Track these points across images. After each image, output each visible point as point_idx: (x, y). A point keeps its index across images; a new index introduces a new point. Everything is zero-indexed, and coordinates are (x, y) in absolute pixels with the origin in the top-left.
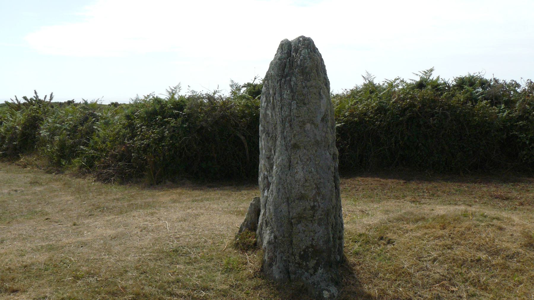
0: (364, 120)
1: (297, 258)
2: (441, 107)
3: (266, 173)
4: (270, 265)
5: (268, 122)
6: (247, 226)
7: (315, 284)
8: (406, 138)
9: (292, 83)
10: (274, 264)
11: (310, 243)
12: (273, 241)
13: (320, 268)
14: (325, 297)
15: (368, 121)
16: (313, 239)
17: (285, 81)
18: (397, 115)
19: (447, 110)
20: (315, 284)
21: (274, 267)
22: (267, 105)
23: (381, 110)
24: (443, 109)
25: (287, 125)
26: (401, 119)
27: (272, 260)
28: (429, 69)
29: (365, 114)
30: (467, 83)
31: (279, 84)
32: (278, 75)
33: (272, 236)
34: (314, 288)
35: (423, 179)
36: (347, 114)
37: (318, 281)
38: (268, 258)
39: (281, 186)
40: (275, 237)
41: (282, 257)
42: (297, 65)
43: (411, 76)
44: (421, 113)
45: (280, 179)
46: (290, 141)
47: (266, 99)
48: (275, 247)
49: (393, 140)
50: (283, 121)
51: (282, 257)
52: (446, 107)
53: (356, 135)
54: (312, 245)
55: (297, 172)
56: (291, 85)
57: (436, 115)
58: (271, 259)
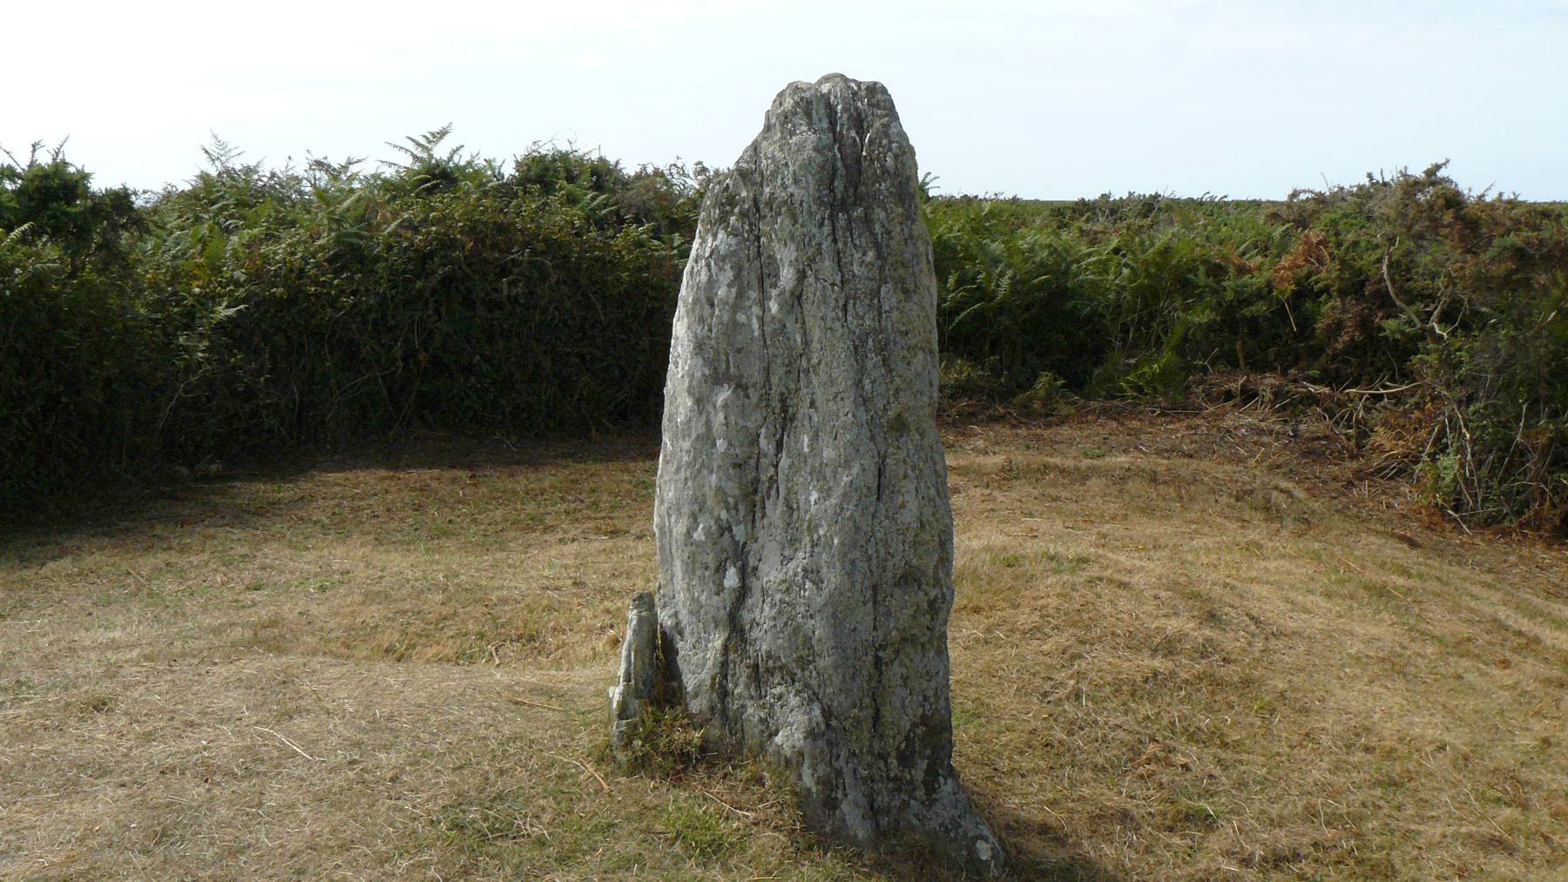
0: (300, 291)
1: (893, 761)
2: (525, 245)
3: (724, 515)
4: (831, 804)
5: (739, 351)
6: (638, 694)
7: (947, 831)
8: (438, 340)
9: (878, 228)
10: (840, 796)
11: (920, 711)
12: (823, 726)
13: (941, 780)
14: (984, 858)
15: (314, 295)
16: (926, 698)
17: (849, 221)
18: (404, 272)
19: (543, 253)
20: (947, 831)
21: (845, 807)
22: (740, 295)
23: (350, 255)
24: (534, 252)
25: (873, 360)
26: (419, 285)
27: (830, 784)
28: (436, 129)
29: (301, 273)
30: (545, 174)
31: (826, 229)
32: (819, 201)
33: (817, 712)
34: (951, 840)
35: (392, 457)
36: (240, 275)
37: (953, 818)
38: (818, 783)
39: (856, 554)
40: (827, 714)
41: (855, 771)
42: (885, 171)
43: (377, 151)
44: (470, 265)
45: (857, 529)
46: (885, 410)
47: (738, 276)
48: (830, 743)
49: (398, 351)
50: (856, 348)
51: (855, 771)
52: (540, 247)
53: (280, 340)
54: (923, 716)
55: (903, 506)
56: (873, 234)
57: (516, 271)
58: (823, 782)
